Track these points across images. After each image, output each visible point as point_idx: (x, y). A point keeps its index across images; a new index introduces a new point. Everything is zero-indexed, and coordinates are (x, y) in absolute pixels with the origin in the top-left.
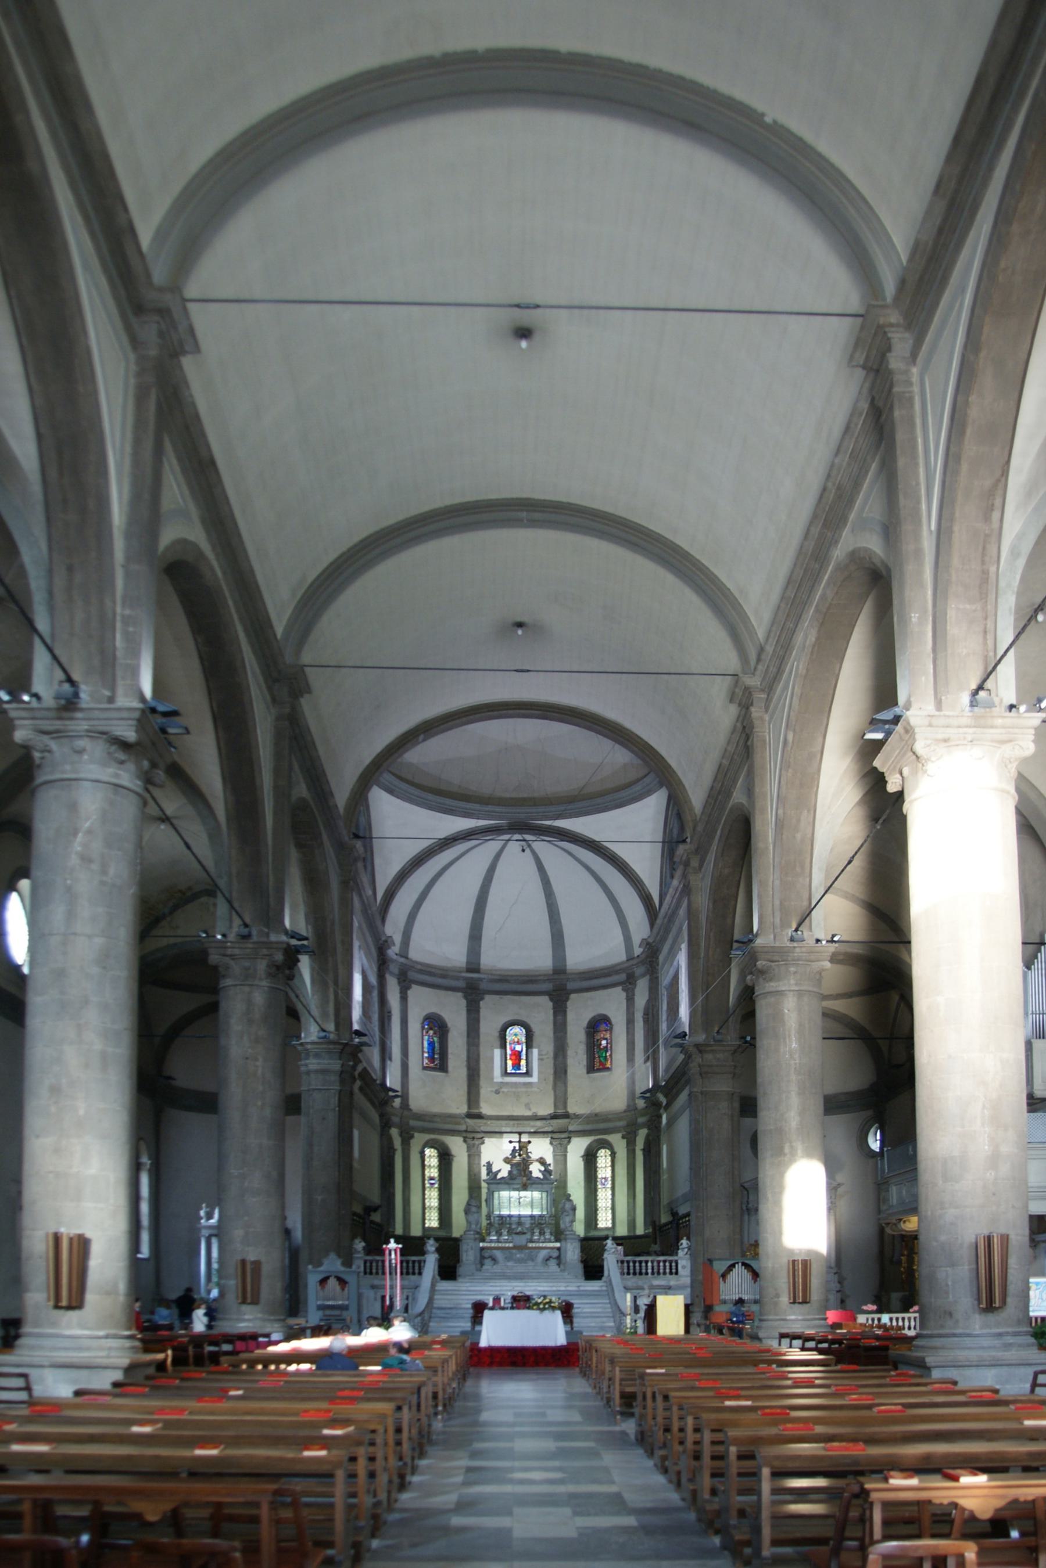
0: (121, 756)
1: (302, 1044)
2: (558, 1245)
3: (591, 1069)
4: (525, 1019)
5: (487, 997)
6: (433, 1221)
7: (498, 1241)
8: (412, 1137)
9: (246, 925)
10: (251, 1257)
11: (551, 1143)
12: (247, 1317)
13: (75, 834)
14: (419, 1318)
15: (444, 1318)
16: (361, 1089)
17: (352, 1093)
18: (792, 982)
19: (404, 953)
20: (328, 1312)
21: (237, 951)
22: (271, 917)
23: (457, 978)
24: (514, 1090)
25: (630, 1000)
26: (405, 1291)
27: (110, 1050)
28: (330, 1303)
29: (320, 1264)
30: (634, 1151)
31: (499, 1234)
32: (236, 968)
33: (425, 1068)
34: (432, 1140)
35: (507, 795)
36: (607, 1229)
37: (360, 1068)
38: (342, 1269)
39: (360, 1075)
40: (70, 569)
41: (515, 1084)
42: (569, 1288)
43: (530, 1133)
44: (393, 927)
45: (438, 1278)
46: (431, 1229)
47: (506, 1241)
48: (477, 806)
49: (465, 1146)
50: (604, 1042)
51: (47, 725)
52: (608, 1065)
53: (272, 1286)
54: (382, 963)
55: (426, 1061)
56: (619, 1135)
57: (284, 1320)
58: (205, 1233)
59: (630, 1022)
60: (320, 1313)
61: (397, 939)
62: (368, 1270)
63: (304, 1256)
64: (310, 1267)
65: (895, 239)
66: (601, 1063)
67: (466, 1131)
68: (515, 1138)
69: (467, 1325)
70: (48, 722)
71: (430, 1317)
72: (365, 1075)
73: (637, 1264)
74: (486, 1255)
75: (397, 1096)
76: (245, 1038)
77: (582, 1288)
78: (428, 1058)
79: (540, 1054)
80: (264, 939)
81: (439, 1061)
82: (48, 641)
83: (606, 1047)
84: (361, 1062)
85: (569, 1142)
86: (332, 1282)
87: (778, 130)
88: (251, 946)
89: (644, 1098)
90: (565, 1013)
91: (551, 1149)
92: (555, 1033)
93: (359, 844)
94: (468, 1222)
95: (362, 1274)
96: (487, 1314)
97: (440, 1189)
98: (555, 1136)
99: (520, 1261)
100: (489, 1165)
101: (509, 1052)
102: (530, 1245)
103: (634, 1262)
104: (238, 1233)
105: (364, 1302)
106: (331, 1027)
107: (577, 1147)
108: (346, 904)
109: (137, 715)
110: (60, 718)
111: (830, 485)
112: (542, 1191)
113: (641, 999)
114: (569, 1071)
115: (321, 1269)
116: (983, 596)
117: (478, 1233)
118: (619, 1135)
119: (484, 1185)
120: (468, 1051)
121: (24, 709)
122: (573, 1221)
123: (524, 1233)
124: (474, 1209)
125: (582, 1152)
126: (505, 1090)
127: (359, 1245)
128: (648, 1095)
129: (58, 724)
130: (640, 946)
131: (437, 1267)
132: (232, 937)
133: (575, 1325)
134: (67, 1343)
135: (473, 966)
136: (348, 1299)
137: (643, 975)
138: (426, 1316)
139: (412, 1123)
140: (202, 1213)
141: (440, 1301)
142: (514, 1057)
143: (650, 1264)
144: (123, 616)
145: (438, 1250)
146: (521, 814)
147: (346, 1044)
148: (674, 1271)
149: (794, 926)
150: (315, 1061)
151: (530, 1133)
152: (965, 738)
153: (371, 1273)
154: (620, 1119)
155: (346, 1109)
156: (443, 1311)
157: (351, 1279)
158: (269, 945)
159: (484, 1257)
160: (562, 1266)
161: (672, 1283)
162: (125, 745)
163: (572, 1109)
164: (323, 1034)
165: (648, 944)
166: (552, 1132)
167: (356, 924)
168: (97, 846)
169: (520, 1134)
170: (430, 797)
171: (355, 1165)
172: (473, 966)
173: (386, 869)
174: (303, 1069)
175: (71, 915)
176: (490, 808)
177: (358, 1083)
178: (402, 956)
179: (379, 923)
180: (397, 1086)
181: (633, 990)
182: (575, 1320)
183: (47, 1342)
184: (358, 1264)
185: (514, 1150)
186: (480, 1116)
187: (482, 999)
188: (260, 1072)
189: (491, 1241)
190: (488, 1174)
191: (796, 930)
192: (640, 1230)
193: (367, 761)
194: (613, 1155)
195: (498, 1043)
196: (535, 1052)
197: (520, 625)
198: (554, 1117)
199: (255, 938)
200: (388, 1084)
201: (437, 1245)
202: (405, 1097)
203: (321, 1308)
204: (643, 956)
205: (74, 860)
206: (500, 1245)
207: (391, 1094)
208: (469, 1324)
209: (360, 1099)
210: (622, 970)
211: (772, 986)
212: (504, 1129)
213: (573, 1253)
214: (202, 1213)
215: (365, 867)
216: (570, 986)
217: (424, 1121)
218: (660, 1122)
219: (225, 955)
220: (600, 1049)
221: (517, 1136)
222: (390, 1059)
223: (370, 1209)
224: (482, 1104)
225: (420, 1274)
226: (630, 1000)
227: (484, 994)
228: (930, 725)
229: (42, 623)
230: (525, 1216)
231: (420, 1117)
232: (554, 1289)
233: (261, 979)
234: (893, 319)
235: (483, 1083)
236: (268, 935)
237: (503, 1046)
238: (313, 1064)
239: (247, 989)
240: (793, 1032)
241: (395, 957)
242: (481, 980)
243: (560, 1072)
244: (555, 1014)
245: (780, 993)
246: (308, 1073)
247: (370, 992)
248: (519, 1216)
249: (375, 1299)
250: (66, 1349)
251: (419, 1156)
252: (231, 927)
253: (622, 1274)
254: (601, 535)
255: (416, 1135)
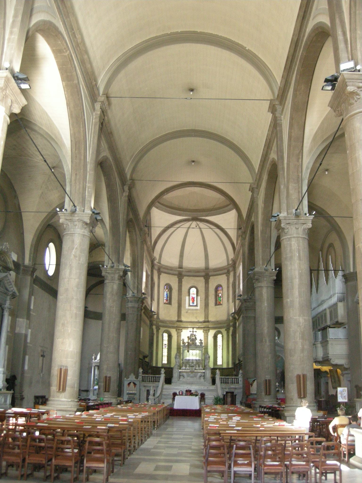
0: (85, 226)
1: (127, 298)
2: (204, 371)
3: (216, 304)
4: (196, 286)
5: (185, 278)
6: (165, 361)
7: (185, 369)
8: (160, 329)
9: (113, 263)
10: (108, 375)
11: (203, 332)
12: (106, 396)
13: (73, 249)
14: (158, 398)
15: (166, 398)
16: (144, 313)
17: (141, 315)
18: (265, 283)
19: (159, 263)
20: (130, 396)
21: (110, 271)
22: (119, 260)
23: (175, 271)
24: (192, 312)
25: (228, 279)
26: (154, 388)
27: (78, 312)
28: (131, 392)
29: (128, 378)
30: (229, 335)
31: (186, 366)
32: (109, 277)
33: (165, 303)
34: (166, 330)
35: (192, 208)
36: (220, 365)
37: (144, 306)
38: (135, 379)
39: (144, 308)
40: (76, 174)
41: (193, 310)
42: (205, 388)
43: (196, 328)
44: (156, 254)
45: (164, 383)
46: (164, 364)
47: (188, 369)
48: (182, 212)
49: (176, 332)
50: (220, 295)
51: (68, 218)
52: (221, 303)
53: (114, 386)
54: (153, 266)
55: (165, 301)
56: (224, 329)
57: (116, 398)
58: (94, 365)
59: (228, 287)
60: (128, 396)
61: (157, 257)
62: (143, 380)
63: (124, 374)
64: (125, 378)
65: (277, 81)
66: (219, 302)
67: (177, 327)
68: (191, 330)
69: (170, 401)
70: (68, 217)
71: (161, 398)
72: (145, 308)
73: (226, 379)
74: (181, 374)
75: (155, 314)
76: (111, 300)
77: (209, 388)
78: (166, 300)
79: (200, 299)
80: (118, 268)
81: (169, 302)
82: (69, 196)
83: (221, 296)
84: (144, 303)
85: (209, 331)
86: (132, 384)
87: (249, 51)
88: (114, 270)
89: (232, 316)
90: (208, 284)
91: (203, 334)
92: (205, 291)
93: (146, 229)
94: (176, 362)
95: (141, 381)
96: (176, 397)
97: (168, 349)
98: (205, 329)
99: (192, 377)
100: (183, 340)
101: (191, 298)
102: (195, 371)
103: (225, 378)
104: (105, 367)
105: (141, 392)
106: (135, 292)
107: (212, 333)
108: (142, 249)
109: (90, 215)
110: (71, 216)
111: (268, 138)
112: (199, 350)
113: (231, 280)
114: (209, 305)
115: (129, 379)
116: (298, 182)
117: (179, 366)
118: (224, 329)
119: (182, 347)
120: (178, 297)
121: (63, 213)
122: (209, 362)
123: (193, 366)
124: (178, 357)
125: (213, 335)
126: (189, 311)
127: (141, 370)
128: (233, 315)
129: (71, 218)
130: (231, 261)
131: (164, 379)
132: (109, 267)
133: (206, 402)
134: (61, 403)
135: (181, 267)
136: (136, 391)
137: (232, 271)
138: (160, 397)
139: (160, 324)
140: (93, 357)
141: (165, 392)
142: (192, 299)
143: (230, 379)
144: (88, 186)
145: (165, 373)
146: (195, 214)
147: (140, 298)
148: (237, 382)
149: (266, 265)
150: (130, 304)
151: (196, 328)
152: (294, 223)
153: (144, 381)
154: (224, 323)
155: (139, 320)
156: (165, 396)
157: (137, 383)
158: (118, 269)
159: (180, 375)
160: (205, 380)
161: (237, 387)
162: (86, 224)
163: (211, 319)
164: (133, 294)
165: (233, 260)
166: (204, 328)
167: (145, 255)
168: (78, 253)
169: (193, 328)
170: (168, 209)
171: (141, 340)
172: (181, 267)
173: (155, 233)
174: (127, 306)
175: (70, 273)
176: (186, 213)
177: (143, 311)
178: (159, 263)
179: (152, 253)
180: (156, 311)
181: (229, 276)
182: (206, 400)
183: (56, 403)
184: (140, 378)
185: (191, 335)
186: (181, 321)
187: (183, 278)
188: (114, 311)
189: (183, 369)
190: (183, 344)
191: (266, 266)
192: (230, 366)
193: (150, 201)
194: (223, 337)
195: (188, 294)
196: (199, 297)
197: (193, 161)
198: (204, 322)
199: (115, 267)
200: (153, 310)
201: (165, 371)
202: (158, 314)
203: (129, 394)
204: (232, 264)
205: (72, 257)
206: (186, 371)
207: (154, 313)
208: (171, 401)
209: (144, 316)
210: (225, 269)
211: (260, 284)
212: (189, 326)
213: (209, 374)
214: (93, 357)
215: (148, 236)
216: (210, 274)
217: (164, 323)
218: (236, 325)
219: (106, 273)
220: (219, 297)
221: (192, 329)
222: (154, 300)
223: (145, 357)
224: (182, 317)
225: (159, 382)
226: (228, 279)
227: (184, 276)
228: (285, 219)
229: (68, 189)
230: (194, 360)
231: (163, 322)
232: (200, 388)
233: (116, 281)
234: (277, 103)
235: (183, 309)
236: (119, 267)
237: (189, 295)
238: (130, 305)
239: (112, 284)
240: (265, 300)
241: (157, 263)
242: (183, 271)
243: (207, 305)
244: (205, 284)
245: (261, 287)
246: (128, 308)
247: (148, 277)
248: (193, 360)
249: (145, 391)
250: (60, 405)
251: (162, 336)
252: (109, 263)
253: (221, 383)
254: (215, 140)
255: (161, 328)
